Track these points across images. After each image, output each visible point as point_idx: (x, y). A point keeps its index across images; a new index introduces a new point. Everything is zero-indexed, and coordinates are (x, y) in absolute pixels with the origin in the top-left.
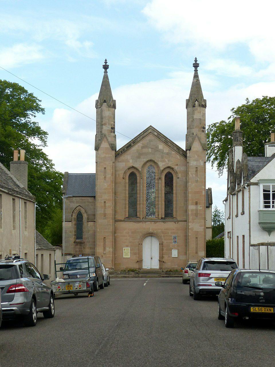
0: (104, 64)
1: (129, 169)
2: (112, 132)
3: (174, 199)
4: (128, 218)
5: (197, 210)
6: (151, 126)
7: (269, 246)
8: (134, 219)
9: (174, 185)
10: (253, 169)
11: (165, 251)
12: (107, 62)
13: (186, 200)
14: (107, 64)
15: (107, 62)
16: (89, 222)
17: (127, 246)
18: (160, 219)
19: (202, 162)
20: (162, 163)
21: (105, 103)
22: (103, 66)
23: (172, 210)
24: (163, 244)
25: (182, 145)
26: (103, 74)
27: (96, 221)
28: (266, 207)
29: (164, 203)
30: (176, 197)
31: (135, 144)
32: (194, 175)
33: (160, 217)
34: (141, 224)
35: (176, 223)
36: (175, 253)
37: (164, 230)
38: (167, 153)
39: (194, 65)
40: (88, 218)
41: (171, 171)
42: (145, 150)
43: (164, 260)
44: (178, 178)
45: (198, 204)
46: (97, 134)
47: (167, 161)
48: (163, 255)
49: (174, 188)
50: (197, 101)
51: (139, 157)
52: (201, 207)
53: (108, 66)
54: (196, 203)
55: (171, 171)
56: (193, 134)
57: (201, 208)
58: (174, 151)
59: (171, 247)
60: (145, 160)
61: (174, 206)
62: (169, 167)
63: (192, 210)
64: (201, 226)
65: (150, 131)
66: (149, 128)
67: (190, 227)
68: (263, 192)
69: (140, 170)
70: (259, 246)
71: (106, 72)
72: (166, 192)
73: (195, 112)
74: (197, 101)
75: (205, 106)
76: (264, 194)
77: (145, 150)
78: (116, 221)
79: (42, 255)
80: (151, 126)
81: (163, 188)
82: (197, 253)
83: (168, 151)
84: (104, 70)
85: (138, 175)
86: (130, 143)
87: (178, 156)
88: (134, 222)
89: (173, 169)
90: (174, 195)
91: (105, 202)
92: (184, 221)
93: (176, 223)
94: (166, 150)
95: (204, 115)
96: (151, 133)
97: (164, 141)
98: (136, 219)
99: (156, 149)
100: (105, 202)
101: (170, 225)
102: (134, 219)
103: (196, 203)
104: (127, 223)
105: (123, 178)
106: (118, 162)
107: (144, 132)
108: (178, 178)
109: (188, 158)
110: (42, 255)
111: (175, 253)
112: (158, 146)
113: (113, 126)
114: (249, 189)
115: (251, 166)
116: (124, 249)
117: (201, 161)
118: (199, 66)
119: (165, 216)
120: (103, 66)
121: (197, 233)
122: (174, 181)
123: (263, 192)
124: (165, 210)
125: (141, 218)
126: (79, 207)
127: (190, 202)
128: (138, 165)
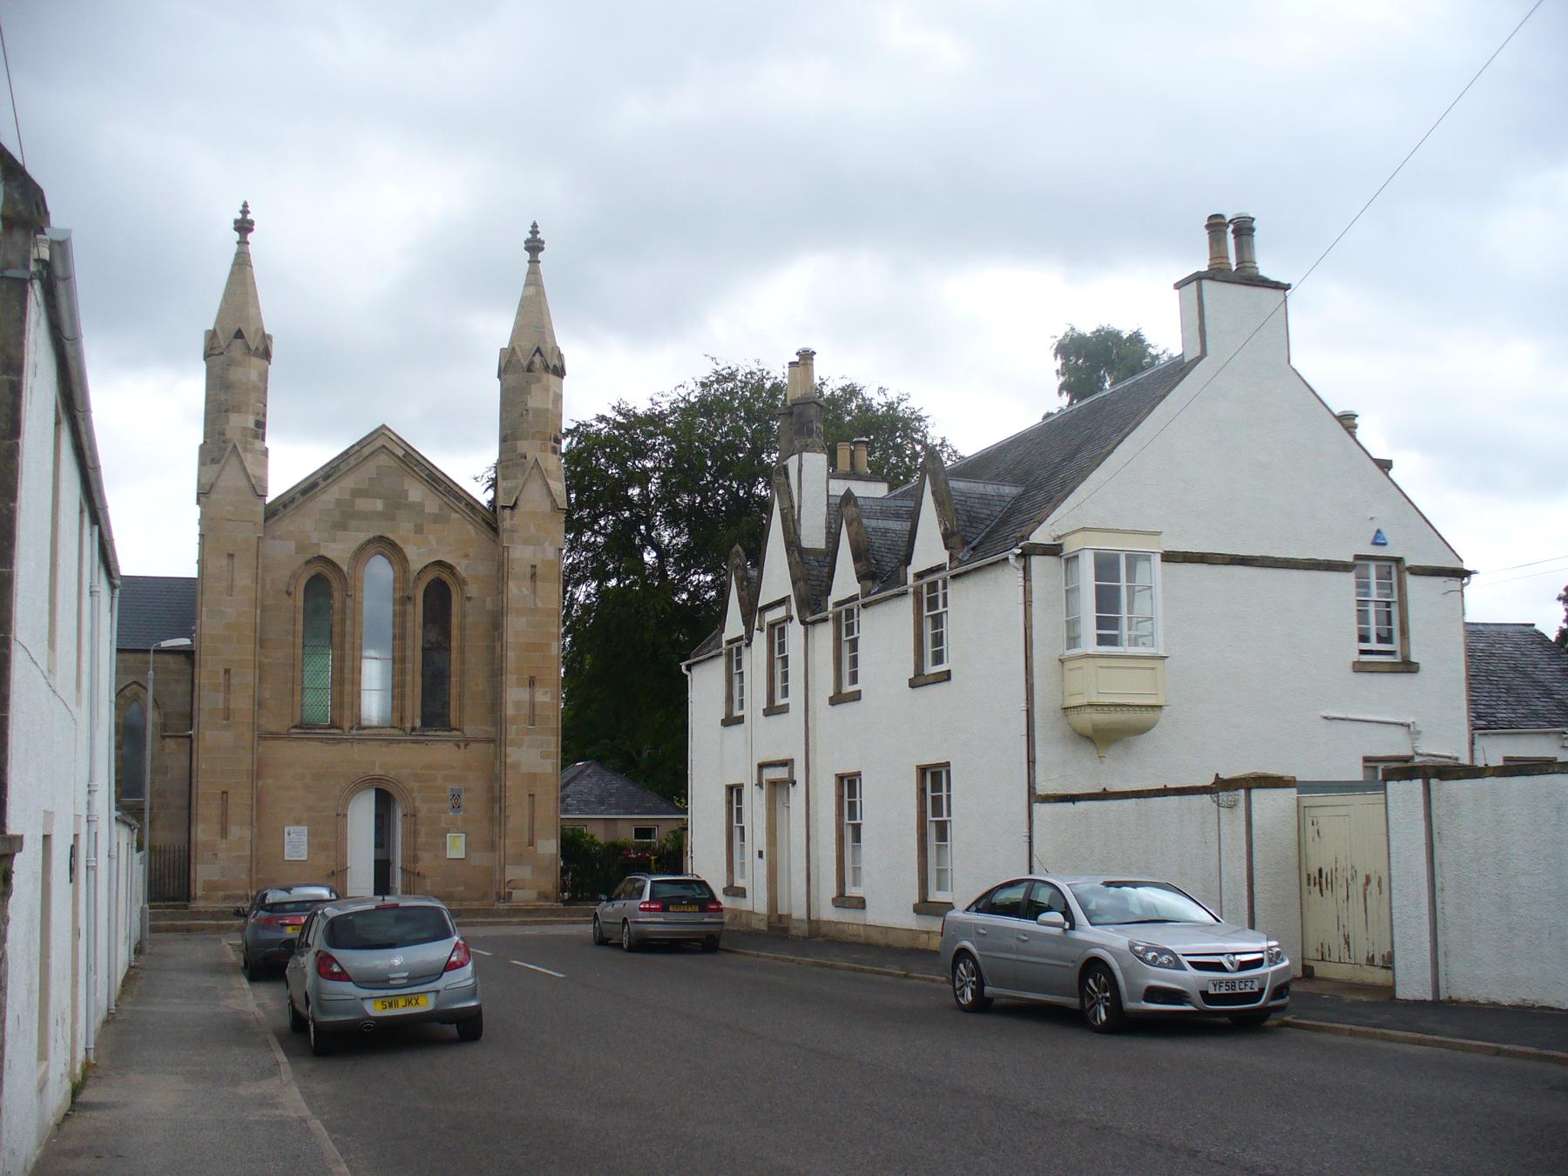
0: (239, 216)
1: (308, 562)
2: (257, 438)
3: (455, 666)
4: (303, 728)
5: (533, 704)
6: (384, 426)
7: (1434, 782)
8: (322, 731)
9: (455, 621)
10: (969, 508)
11: (422, 839)
12: (249, 212)
13: (496, 673)
14: (249, 217)
15: (249, 212)
16: (167, 739)
17: (298, 822)
18: (409, 731)
19: (552, 547)
20: (418, 549)
21: (239, 340)
22: (236, 222)
23: (446, 705)
24: (419, 815)
25: (484, 497)
26: (234, 248)
27: (1109, 544)
28: (1102, 640)
29: (419, 679)
30: (463, 662)
31: (330, 481)
32: (524, 590)
33: (408, 725)
34: (344, 747)
35: (459, 748)
36: (456, 847)
37: (421, 769)
38: (436, 515)
39: (531, 244)
40: (164, 727)
41: (445, 577)
42: (362, 504)
43: (420, 867)
44: (469, 600)
45: (537, 684)
46: (205, 442)
47: (434, 543)
48: (419, 853)
49: (455, 632)
50: (538, 354)
51: (341, 526)
52: (546, 693)
53: (252, 223)
54: (532, 682)
55: (447, 577)
56: (526, 458)
57: (547, 699)
58: (457, 512)
59: (443, 825)
60: (363, 537)
61: (454, 691)
62: (440, 563)
63: (518, 704)
64: (545, 756)
65: (379, 443)
66: (380, 433)
67: (508, 760)
68: (1096, 581)
69: (345, 568)
70: (1248, 790)
71: (243, 242)
72: (427, 646)
73: (533, 386)
74: (538, 354)
75: (560, 372)
76: (1097, 586)
77: (362, 504)
78: (266, 736)
79: (730, 788)
80: (384, 426)
81: (419, 632)
82: (531, 843)
83: (436, 511)
84: (236, 236)
85: (336, 585)
86: (314, 478)
87: (470, 527)
88: (321, 740)
89: (450, 568)
90: (454, 655)
91: (227, 671)
92: (489, 741)
93: (459, 748)
94: (432, 505)
95: (558, 398)
96: (384, 450)
97: (426, 478)
98: (329, 731)
99: (397, 503)
100: (227, 671)
101: (440, 754)
102: (322, 731)
103: (532, 682)
104: (295, 744)
105: (289, 594)
106: (274, 538)
107: (365, 443)
108: (469, 599)
109: (505, 536)
110: (730, 788)
111: (456, 847)
112: (407, 490)
113: (260, 418)
114: (1026, 571)
115: (961, 498)
116: (286, 833)
117: (547, 544)
118: (542, 249)
119: (424, 724)
120: (236, 222)
121: (533, 778)
122: (455, 609)
123: (1096, 581)
124: (424, 704)
125: (347, 730)
126: (135, 686)
127: (510, 678)
128: (339, 550)
